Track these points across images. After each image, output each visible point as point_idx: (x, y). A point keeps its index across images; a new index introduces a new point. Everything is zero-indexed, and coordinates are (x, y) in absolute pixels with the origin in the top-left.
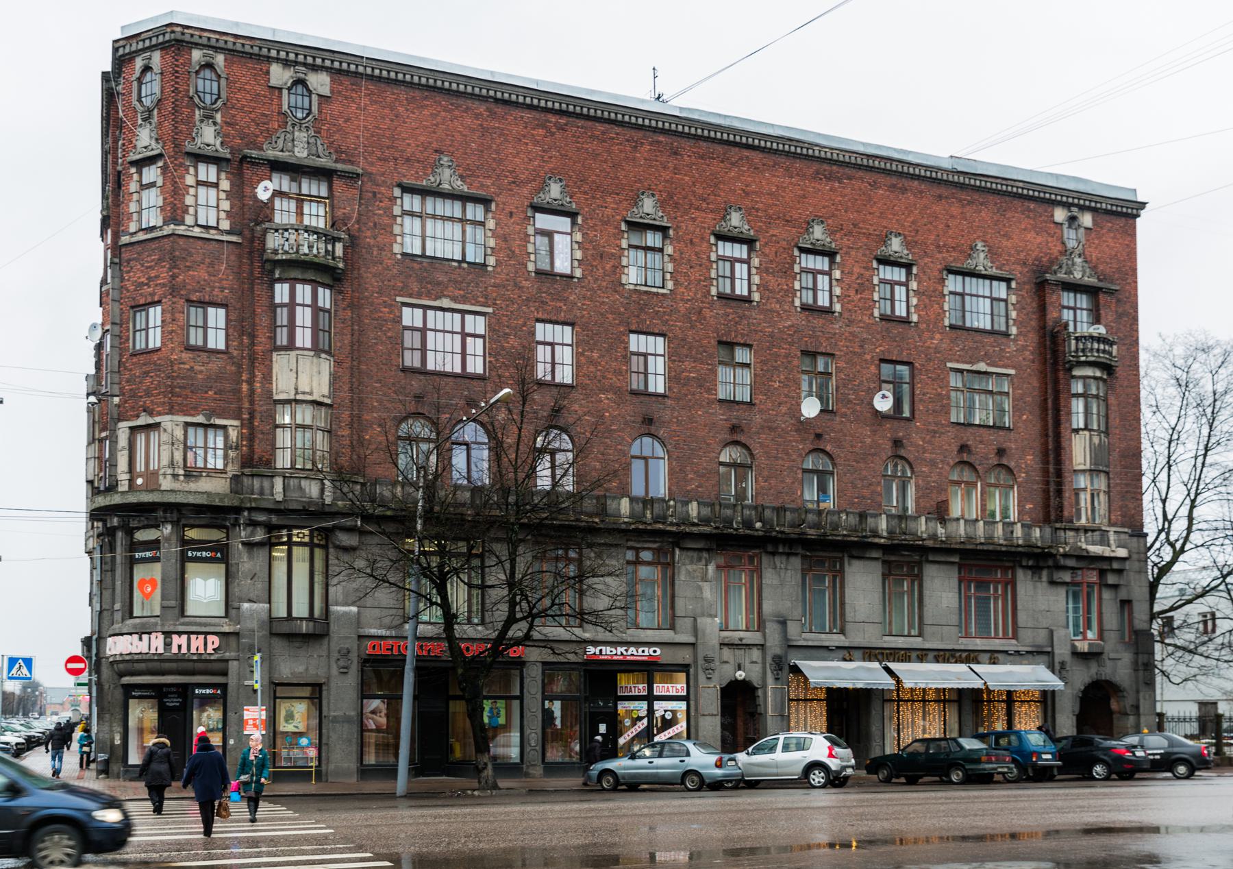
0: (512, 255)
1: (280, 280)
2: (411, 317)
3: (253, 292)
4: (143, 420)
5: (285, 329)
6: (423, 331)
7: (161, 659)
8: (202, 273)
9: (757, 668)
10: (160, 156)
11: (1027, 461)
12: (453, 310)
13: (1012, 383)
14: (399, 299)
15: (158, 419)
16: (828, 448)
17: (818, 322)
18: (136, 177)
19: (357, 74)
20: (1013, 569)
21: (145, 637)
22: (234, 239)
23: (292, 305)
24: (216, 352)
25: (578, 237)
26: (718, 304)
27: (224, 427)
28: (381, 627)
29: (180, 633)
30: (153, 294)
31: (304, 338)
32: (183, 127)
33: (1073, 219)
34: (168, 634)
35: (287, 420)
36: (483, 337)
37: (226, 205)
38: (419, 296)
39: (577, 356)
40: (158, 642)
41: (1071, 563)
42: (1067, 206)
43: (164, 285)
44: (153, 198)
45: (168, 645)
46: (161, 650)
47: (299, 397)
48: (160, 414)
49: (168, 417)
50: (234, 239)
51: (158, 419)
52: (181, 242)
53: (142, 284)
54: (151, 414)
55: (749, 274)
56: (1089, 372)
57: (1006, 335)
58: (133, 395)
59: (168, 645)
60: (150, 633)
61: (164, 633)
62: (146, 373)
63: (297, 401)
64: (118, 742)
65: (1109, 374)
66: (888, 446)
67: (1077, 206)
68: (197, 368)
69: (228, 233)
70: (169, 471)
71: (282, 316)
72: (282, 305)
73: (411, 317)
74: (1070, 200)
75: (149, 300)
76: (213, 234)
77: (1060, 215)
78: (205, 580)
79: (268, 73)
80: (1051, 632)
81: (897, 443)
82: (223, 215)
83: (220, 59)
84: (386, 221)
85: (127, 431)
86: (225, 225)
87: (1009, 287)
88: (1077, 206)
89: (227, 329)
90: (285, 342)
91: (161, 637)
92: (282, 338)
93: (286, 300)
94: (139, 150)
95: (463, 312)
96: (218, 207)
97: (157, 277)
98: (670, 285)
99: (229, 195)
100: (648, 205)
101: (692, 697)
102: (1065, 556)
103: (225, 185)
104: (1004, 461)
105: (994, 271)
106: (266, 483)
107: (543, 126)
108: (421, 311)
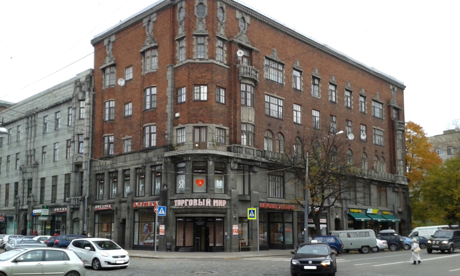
0: (289, 82)
1: (243, 83)
2: (267, 98)
3: (236, 86)
4: (200, 124)
5: (244, 99)
6: (269, 103)
7: (209, 208)
8: (219, 77)
9: (340, 214)
10: (207, 35)
11: (387, 156)
12: (276, 98)
13: (383, 133)
14: (265, 92)
15: (207, 125)
16: (351, 149)
17: (349, 111)
18: (195, 40)
19: (256, 18)
20: (386, 187)
21: (204, 200)
22: (228, 67)
23: (246, 92)
24: (222, 104)
25: (302, 79)
26: (330, 103)
27: (225, 130)
28: (263, 198)
29: (216, 199)
30: (204, 82)
31: (249, 103)
32: (215, 27)
33: (393, 89)
34: (212, 199)
35: (245, 129)
36: (382, 136)
37: (225, 55)
38: (269, 92)
39: (302, 115)
40: (208, 202)
41: (398, 186)
42: (393, 85)
43: (209, 79)
44: (183, 51)
45: (212, 203)
46: (210, 205)
47: (249, 122)
48: (207, 123)
49: (211, 125)
50: (228, 67)
51: (207, 125)
52: (215, 66)
53: (199, 78)
54: (203, 122)
55: (223, 53)
56: (248, 82)
57: (383, 120)
58: (195, 115)
59: (212, 203)
60: (206, 199)
61: (211, 199)
62: (201, 109)
63: (248, 123)
64: (174, 238)
65: (255, 85)
66: (362, 149)
67: (245, 13)
68: (219, 109)
69: (226, 65)
70: (211, 143)
71: (243, 95)
72: (243, 91)
73: (267, 98)
74: (248, 12)
75: (202, 83)
76: (222, 64)
77: (391, 87)
78: (219, 180)
79: (235, 13)
80: (394, 206)
81: (364, 148)
82: (224, 58)
83: (248, 19)
84: (262, 66)
85: (192, 127)
86: (225, 62)
87: (383, 106)
88: (245, 13)
89: (225, 96)
90: (244, 104)
91: (210, 200)
92: (243, 102)
93: (244, 90)
94: (197, 31)
95: (278, 98)
96: (223, 55)
97: (206, 76)
98: (321, 96)
99: (227, 52)
100: (298, 64)
101: (328, 223)
102: (397, 184)
103: (225, 49)
104: (270, 128)
105: (279, 60)
106: (241, 150)
107: (295, 43)
108: (277, 99)
